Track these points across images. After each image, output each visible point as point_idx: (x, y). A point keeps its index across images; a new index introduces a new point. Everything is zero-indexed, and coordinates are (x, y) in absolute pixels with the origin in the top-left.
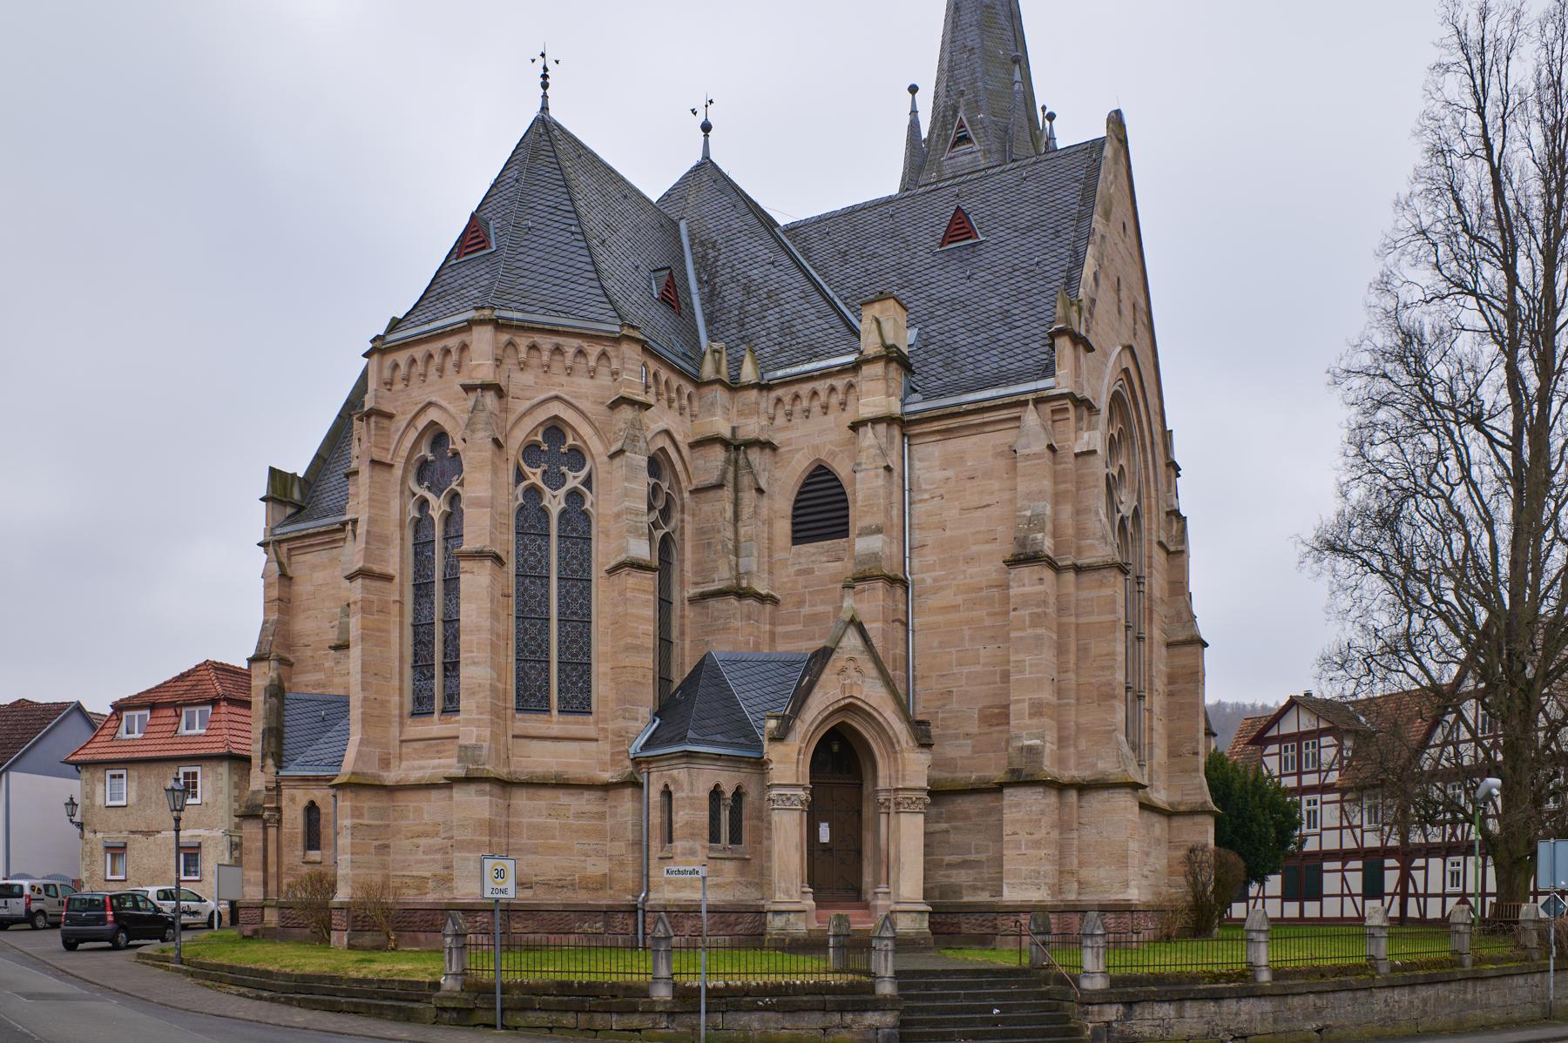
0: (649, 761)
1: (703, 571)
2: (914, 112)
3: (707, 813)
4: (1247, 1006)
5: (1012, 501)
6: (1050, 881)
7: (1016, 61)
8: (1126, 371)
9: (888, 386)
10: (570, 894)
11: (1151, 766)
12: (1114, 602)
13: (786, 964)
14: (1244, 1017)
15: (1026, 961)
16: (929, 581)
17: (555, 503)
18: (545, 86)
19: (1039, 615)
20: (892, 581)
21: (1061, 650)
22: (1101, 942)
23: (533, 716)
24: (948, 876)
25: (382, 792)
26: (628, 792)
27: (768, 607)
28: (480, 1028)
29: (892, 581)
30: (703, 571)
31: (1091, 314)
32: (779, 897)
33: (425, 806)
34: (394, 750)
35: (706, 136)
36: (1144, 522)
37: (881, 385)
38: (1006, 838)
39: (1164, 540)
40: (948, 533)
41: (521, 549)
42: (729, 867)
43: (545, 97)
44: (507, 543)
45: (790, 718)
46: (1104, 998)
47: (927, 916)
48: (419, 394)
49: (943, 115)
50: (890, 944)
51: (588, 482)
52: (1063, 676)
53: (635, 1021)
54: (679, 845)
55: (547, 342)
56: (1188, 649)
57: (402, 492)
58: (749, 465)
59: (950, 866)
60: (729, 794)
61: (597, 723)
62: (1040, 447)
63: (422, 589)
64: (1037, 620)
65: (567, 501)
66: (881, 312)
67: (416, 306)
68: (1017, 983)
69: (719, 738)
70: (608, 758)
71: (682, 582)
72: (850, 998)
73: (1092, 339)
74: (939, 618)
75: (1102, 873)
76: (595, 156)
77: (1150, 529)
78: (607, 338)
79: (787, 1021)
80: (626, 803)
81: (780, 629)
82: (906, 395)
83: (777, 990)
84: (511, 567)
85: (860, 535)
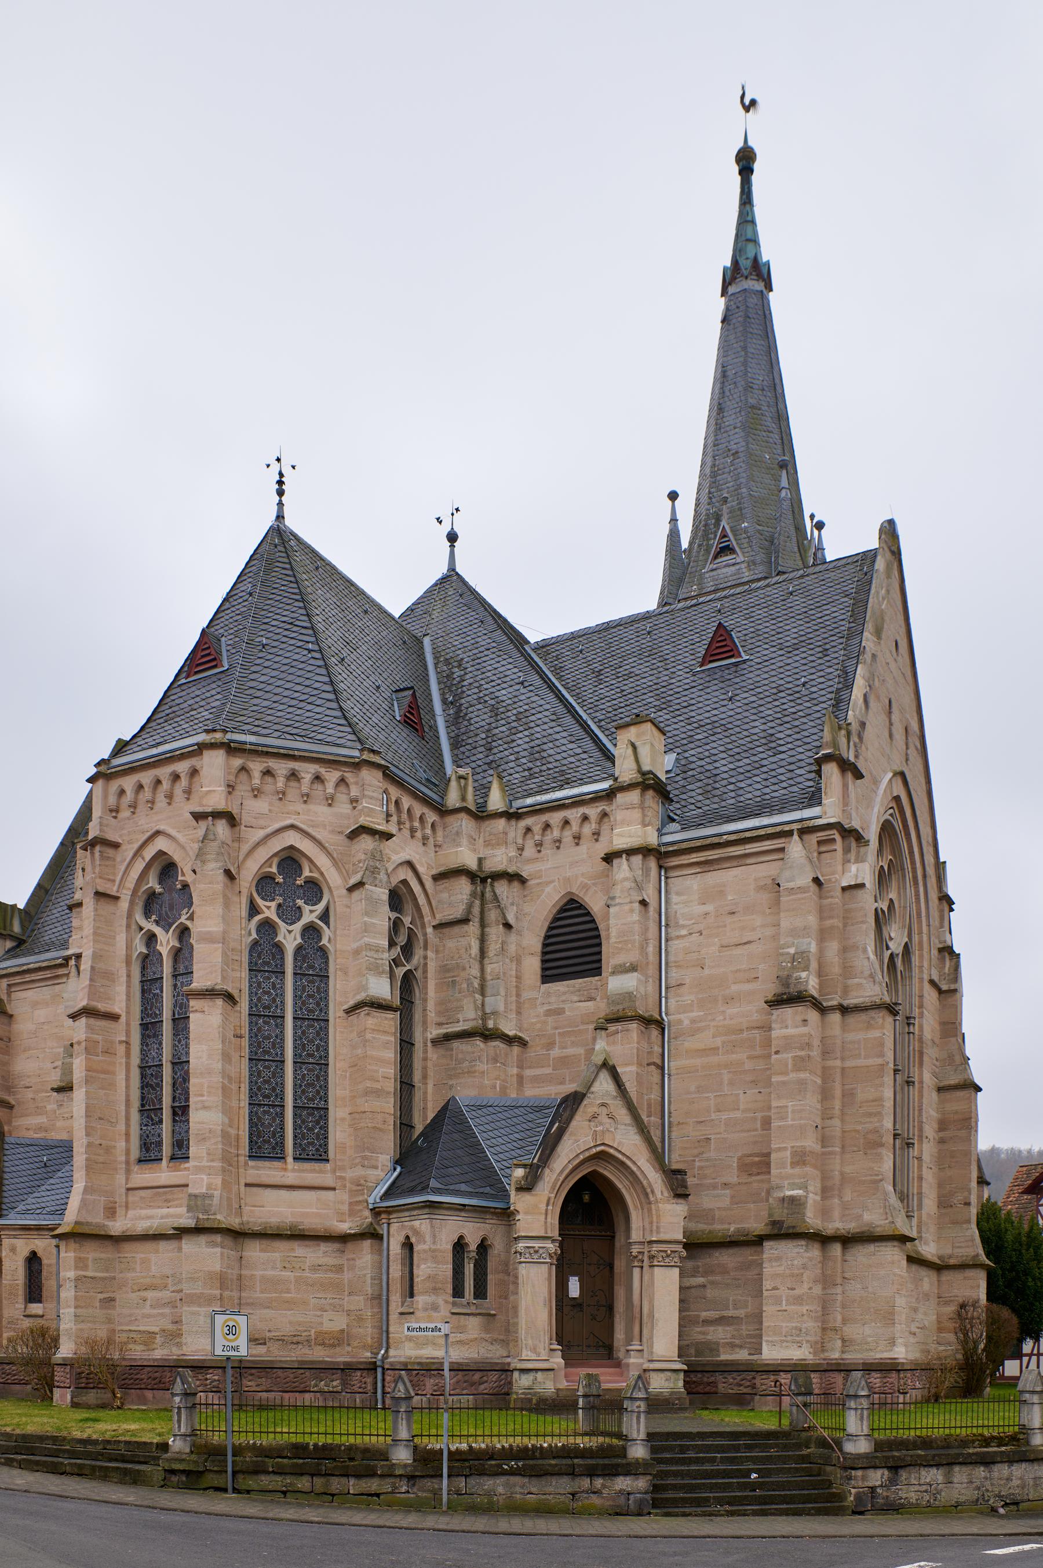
0: (389, 1211)
1: (447, 1011)
2: (674, 520)
4: (1019, 1470)
5: (775, 937)
7: (783, 465)
8: (897, 799)
9: (644, 816)
11: (920, 1218)
12: (882, 1045)
15: (786, 1422)
16: (686, 1022)
17: (290, 938)
18: (281, 493)
19: (802, 1059)
21: (825, 1094)
22: (865, 1403)
23: (267, 1164)
24: (704, 1333)
25: (107, 1243)
26: (367, 1244)
27: (516, 1049)
28: (211, 1492)
30: (447, 1011)
32: (526, 1354)
33: (153, 1257)
34: (120, 1197)
35: (452, 546)
36: (915, 960)
37: (636, 814)
38: (765, 1293)
39: (936, 978)
40: (707, 971)
42: (474, 1323)
43: (280, 504)
44: (239, 981)
46: (868, 1462)
48: (146, 822)
50: (643, 1405)
51: (325, 916)
52: (828, 1122)
53: (373, 1485)
55: (281, 767)
57: (128, 926)
58: (496, 898)
59: (707, 1322)
60: (473, 1247)
61: (334, 1171)
62: (804, 880)
63: (150, 1029)
64: (801, 1063)
65: (303, 936)
66: (638, 736)
67: (143, 728)
68: (777, 1445)
69: (463, 1187)
70: (345, 1208)
71: (425, 1023)
72: (601, 1462)
73: (861, 765)
74: (698, 1062)
75: (867, 1330)
76: (334, 568)
77: (921, 967)
78: (345, 763)
80: (365, 1255)
81: (528, 1073)
82: (663, 825)
83: (523, 1453)
84: (244, 1006)
85: (613, 973)
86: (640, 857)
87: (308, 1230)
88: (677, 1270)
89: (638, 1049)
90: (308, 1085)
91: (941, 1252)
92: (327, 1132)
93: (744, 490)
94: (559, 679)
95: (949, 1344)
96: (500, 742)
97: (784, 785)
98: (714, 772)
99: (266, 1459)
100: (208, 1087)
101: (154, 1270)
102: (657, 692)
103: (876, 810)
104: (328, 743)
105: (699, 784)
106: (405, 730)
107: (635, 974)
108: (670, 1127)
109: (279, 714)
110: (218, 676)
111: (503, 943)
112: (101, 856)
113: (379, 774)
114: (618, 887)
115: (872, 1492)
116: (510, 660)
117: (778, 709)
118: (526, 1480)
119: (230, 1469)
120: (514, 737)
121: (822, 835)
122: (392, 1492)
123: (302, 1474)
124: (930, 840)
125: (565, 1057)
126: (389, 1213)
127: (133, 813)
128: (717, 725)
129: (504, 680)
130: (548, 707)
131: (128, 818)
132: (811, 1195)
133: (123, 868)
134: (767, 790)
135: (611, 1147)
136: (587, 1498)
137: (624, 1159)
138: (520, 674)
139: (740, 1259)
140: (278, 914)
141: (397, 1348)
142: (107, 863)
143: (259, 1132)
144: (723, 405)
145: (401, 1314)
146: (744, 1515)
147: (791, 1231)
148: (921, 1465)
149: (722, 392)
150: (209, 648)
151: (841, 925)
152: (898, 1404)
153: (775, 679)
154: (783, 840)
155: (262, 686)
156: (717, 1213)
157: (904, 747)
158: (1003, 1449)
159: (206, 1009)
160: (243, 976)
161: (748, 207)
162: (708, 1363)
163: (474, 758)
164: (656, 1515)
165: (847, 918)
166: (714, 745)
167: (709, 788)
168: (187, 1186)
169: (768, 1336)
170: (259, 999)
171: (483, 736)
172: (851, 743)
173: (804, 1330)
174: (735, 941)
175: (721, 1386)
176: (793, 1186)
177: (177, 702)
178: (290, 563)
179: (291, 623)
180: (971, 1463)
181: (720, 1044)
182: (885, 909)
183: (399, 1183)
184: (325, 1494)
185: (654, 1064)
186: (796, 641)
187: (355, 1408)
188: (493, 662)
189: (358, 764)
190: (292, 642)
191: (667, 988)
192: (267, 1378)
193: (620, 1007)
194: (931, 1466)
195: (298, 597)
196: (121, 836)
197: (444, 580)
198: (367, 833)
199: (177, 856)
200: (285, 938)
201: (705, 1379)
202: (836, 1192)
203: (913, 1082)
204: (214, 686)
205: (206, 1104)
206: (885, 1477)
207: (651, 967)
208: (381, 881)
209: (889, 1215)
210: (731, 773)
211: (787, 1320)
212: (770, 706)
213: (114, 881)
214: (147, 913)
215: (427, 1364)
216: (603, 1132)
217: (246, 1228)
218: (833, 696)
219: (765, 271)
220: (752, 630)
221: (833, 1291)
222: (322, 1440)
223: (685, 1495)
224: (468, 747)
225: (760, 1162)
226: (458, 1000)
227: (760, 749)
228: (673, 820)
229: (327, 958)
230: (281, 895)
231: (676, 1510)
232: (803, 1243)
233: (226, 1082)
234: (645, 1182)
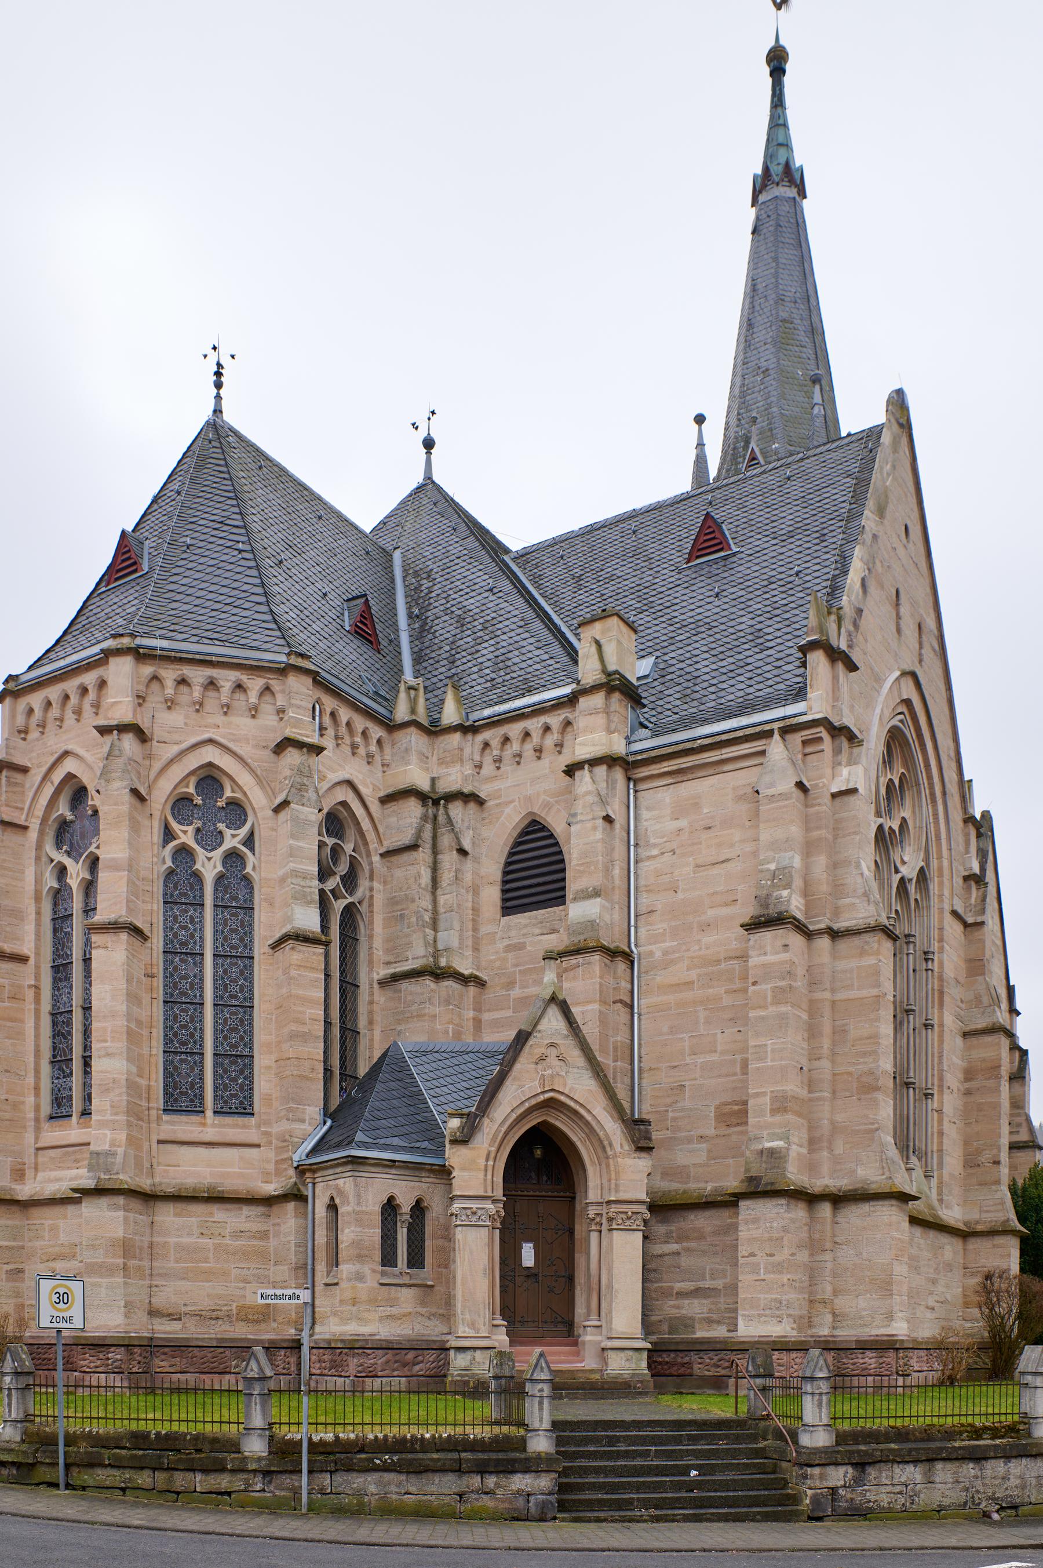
0: (314, 1169)
1: (396, 948)
2: (700, 445)
3: (378, 1231)
4: (1018, 1468)
5: (755, 853)
6: (796, 1312)
7: (816, 380)
8: (907, 702)
9: (609, 721)
11: (940, 1177)
12: (878, 973)
14: (1014, 1482)
15: (743, 1409)
16: (658, 954)
17: (209, 866)
18: (218, 385)
19: (782, 990)
20: (613, 954)
21: (812, 1032)
22: (824, 1386)
23: (184, 1118)
24: (678, 1307)
25: (14, 1208)
26: (291, 1206)
27: (472, 990)
28: (42, 1487)
29: (613, 954)
31: (856, 625)
32: (462, 1330)
33: (61, 1223)
34: (29, 1159)
35: (429, 453)
36: (934, 887)
37: (600, 720)
38: (741, 1261)
39: (960, 911)
40: (680, 895)
41: (170, 922)
42: (407, 1295)
43: (218, 397)
44: (151, 914)
45: (476, 1116)
46: (828, 1458)
47: (645, 1354)
48: (55, 742)
49: (736, 450)
50: (547, 1389)
51: (249, 841)
52: (816, 1064)
53: (223, 1481)
54: (346, 1269)
55: (198, 675)
56: (988, 1039)
57: (38, 858)
58: (450, 821)
59: (681, 1295)
60: (406, 1208)
61: (258, 1126)
62: (787, 785)
63: (61, 971)
64: (780, 995)
65: (224, 863)
66: (603, 632)
67: (58, 642)
68: (727, 1437)
69: (396, 1141)
70: (271, 1167)
71: (371, 962)
72: (494, 1456)
73: (856, 657)
74: (671, 998)
75: (862, 1303)
76: (283, 470)
77: (941, 896)
78: (269, 669)
80: (288, 1216)
81: (486, 1016)
82: (633, 731)
83: (400, 1445)
84: (157, 942)
85: (575, 899)
86: (604, 767)
87: (228, 1192)
88: (640, 1235)
89: (601, 984)
90: (232, 1030)
91: (967, 1218)
92: (252, 1082)
93: (775, 409)
94: (538, 588)
95: (976, 1320)
96: (464, 654)
97: (770, 683)
98: (695, 674)
99: (103, 1451)
100: (112, 1031)
101: (63, 1238)
102: (640, 594)
103: (878, 711)
104: (252, 648)
105: (678, 688)
106: (356, 641)
107: (599, 900)
108: (640, 1073)
109: (200, 618)
110: (137, 581)
111: (456, 871)
112: (8, 781)
113: (309, 681)
114: (580, 803)
115: (833, 1494)
116: (481, 567)
117: (768, 602)
118: (403, 1477)
119: (61, 1461)
120: (479, 647)
121: (807, 733)
122: (245, 1491)
123: (142, 1468)
124: (952, 754)
125: (527, 997)
126: (314, 1171)
127: (42, 733)
128: (701, 623)
129: (474, 586)
130: (517, 612)
131: (38, 740)
132: (794, 1147)
133: (31, 794)
134: (751, 690)
136: (477, 1500)
137: (577, 1107)
138: (490, 581)
139: (717, 1222)
140: (196, 840)
141: (323, 1324)
143: (176, 1083)
144: (753, 321)
145: (327, 1285)
146: (673, 1521)
147: (769, 1188)
148: (893, 1461)
149: (753, 307)
150: (129, 551)
151: (830, 837)
152: (896, 1387)
153: (767, 570)
154: (763, 742)
155: (183, 589)
156: (692, 1169)
157: (917, 646)
158: (998, 1442)
159: (109, 945)
160: (155, 907)
161: (779, 109)
162: (683, 1342)
163: (436, 673)
164: (563, 1520)
165: (837, 830)
166: (697, 645)
167: (689, 691)
168: (88, 1144)
169: (745, 1309)
170: (175, 935)
171: (447, 648)
172: (843, 630)
173: (784, 1303)
175: (696, 1367)
176: (773, 1137)
177: (94, 611)
178: (225, 459)
179: (221, 522)
180: (957, 1459)
181: (695, 978)
182: (896, 828)
183: (329, 1138)
184: (169, 1491)
185: (621, 1001)
186: (791, 528)
187: (280, 1391)
188: (463, 570)
189: (284, 669)
190: (221, 542)
191: (636, 916)
192: (182, 1357)
193: (581, 938)
194: (908, 1462)
195: (231, 495)
196: (30, 760)
197: (419, 489)
198: (294, 746)
199: (86, 779)
200: (203, 866)
201: (679, 1360)
202: (825, 1144)
203: (932, 1026)
204: (132, 591)
205: (110, 1051)
206: (849, 1476)
207: (617, 892)
208: (309, 800)
209: (886, 1170)
210: (713, 674)
211: (765, 1287)
212: (759, 599)
213: (22, 809)
214: (59, 844)
215: (351, 1341)
216: (552, 1076)
217: (158, 1190)
218: (829, 583)
219: (797, 177)
220: (745, 520)
221: (822, 1258)
222: (164, 1429)
223: (605, 1496)
224: (431, 661)
225: (740, 1111)
226: (408, 936)
227: (746, 646)
228: (646, 727)
229: (252, 888)
230: (215, 825)
231: (589, 1514)
232: (783, 1201)
233: (133, 1026)
234: (601, 1134)
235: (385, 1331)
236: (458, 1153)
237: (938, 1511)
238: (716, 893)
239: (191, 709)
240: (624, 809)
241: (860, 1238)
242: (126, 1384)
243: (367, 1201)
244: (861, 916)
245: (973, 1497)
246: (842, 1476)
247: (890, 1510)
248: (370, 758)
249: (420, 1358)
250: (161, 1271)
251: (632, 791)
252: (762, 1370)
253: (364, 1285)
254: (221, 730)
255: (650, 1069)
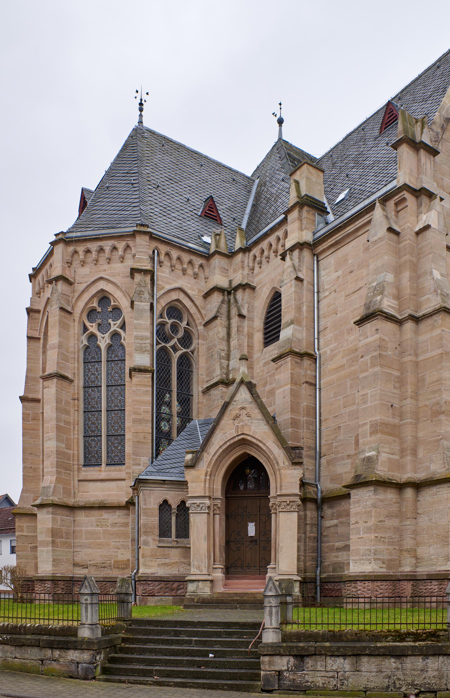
1: (210, 373)
10: (109, 571)
13: (427, 617)
14: (431, 673)
17: (104, 341)
18: (141, 110)
20: (302, 355)
24: (337, 557)
30: (210, 373)
32: (193, 570)
40: (339, 315)
43: (141, 115)
44: (75, 369)
46: (275, 651)
55: (94, 246)
58: (236, 301)
59: (339, 549)
60: (174, 506)
75: (432, 550)
79: (18, 652)
87: (108, 504)
88: (296, 514)
107: (292, 326)
115: (279, 675)
118: (13, 648)
135: (249, 435)
137: (258, 443)
140: (99, 330)
142: (35, 321)
148: (326, 655)
156: (344, 476)
169: (353, 556)
170: (89, 378)
174: (353, 290)
180: (379, 655)
193: (284, 349)
194: (338, 656)
198: (137, 272)
205: (50, 437)
208: (145, 299)
216: (243, 426)
230: (107, 320)
232: (372, 488)
235: (161, 572)
236: (190, 473)
237: (365, 692)
238: (355, 309)
239: (93, 264)
240: (310, 272)
241: (431, 509)
242: (51, 598)
243: (150, 503)
244: (433, 304)
245: (394, 683)
246: (285, 663)
247: (324, 688)
248: (196, 276)
249: (182, 586)
250: (79, 544)
251: (315, 261)
252: (284, 591)
253: (148, 547)
254: (107, 272)
255: (325, 420)
